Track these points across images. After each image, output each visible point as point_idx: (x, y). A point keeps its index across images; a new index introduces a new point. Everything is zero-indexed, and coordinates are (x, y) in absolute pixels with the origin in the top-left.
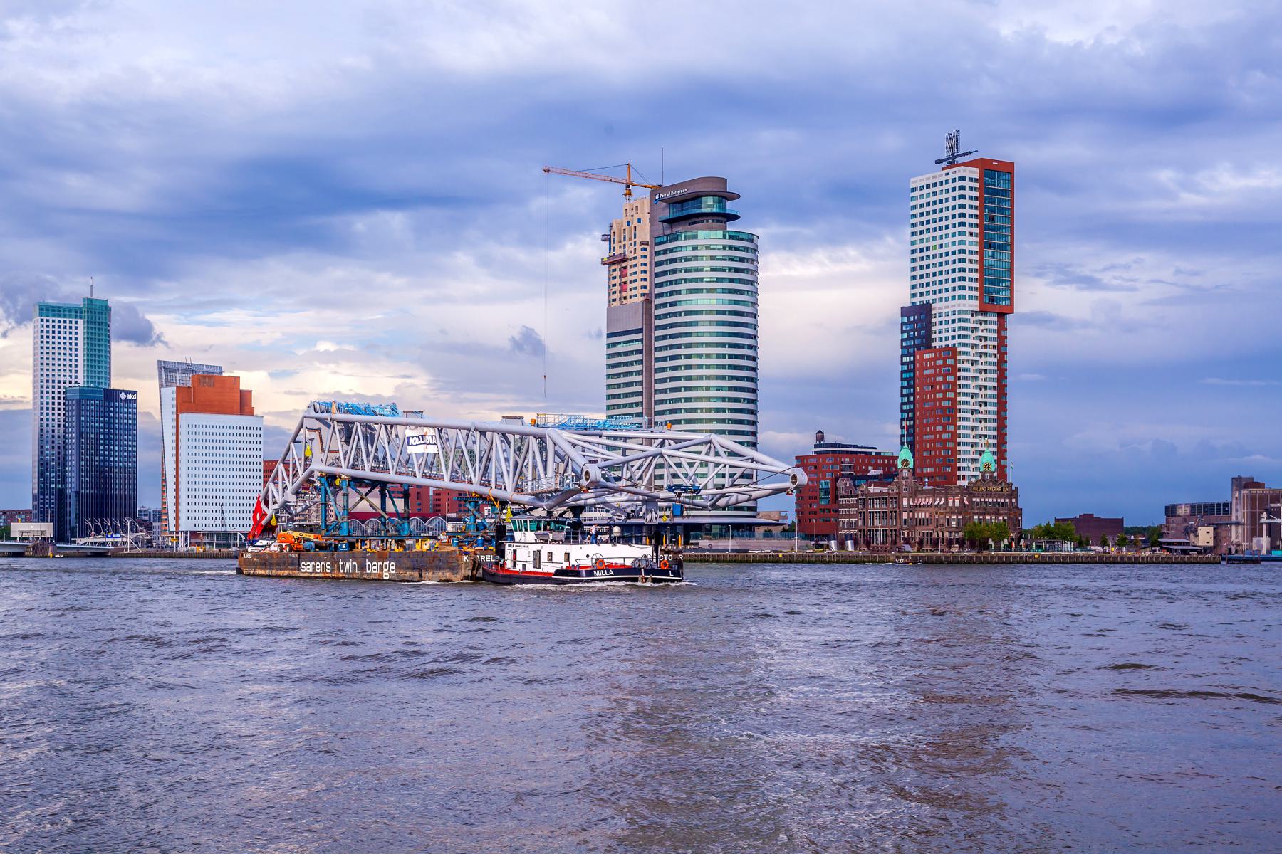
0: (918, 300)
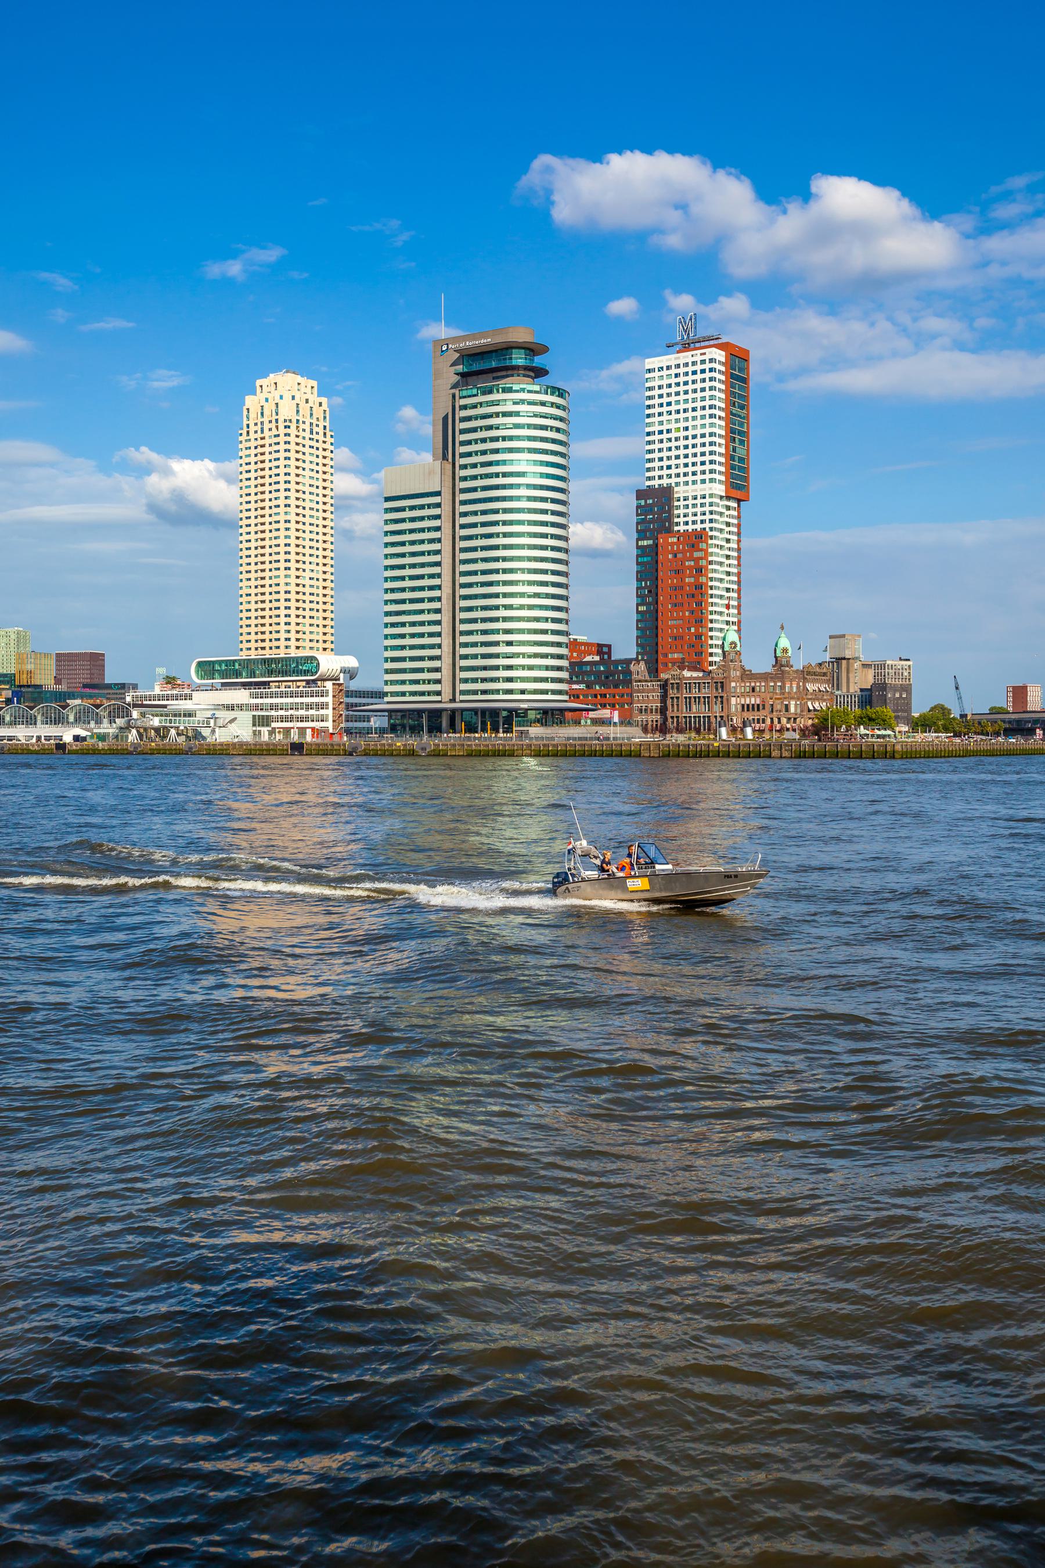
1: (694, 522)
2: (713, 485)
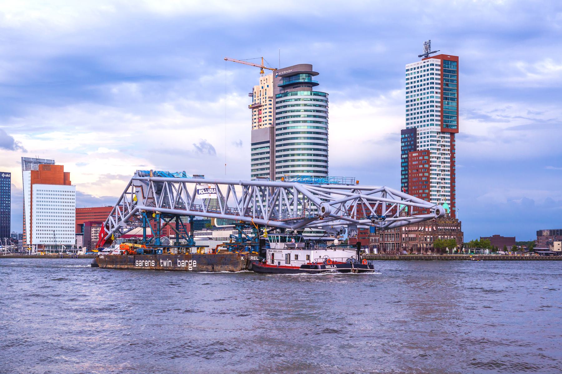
0: (410, 126)
1: (424, 146)
2: (432, 127)
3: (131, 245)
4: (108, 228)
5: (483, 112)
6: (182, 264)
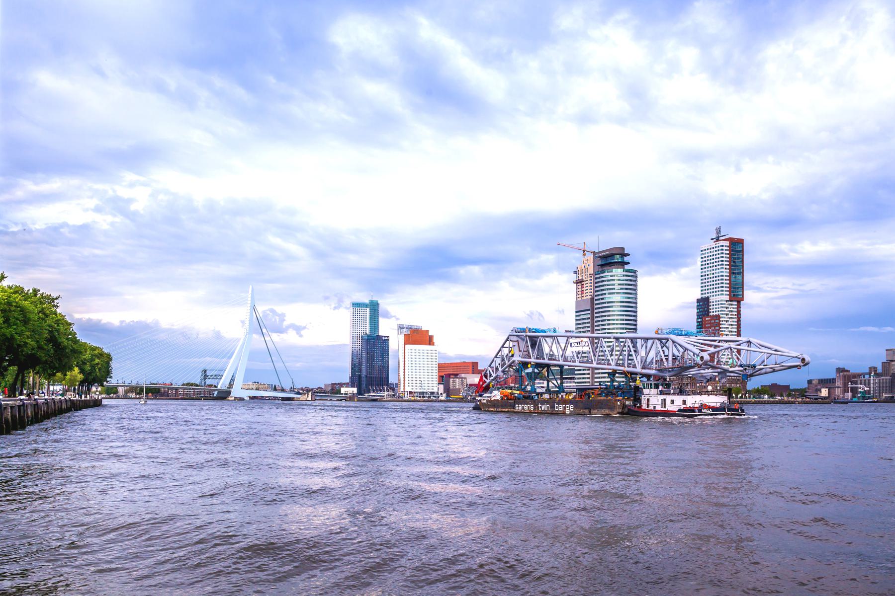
0: (704, 296)
3: (510, 391)
4: (486, 377)
5: (755, 285)
6: (560, 408)
